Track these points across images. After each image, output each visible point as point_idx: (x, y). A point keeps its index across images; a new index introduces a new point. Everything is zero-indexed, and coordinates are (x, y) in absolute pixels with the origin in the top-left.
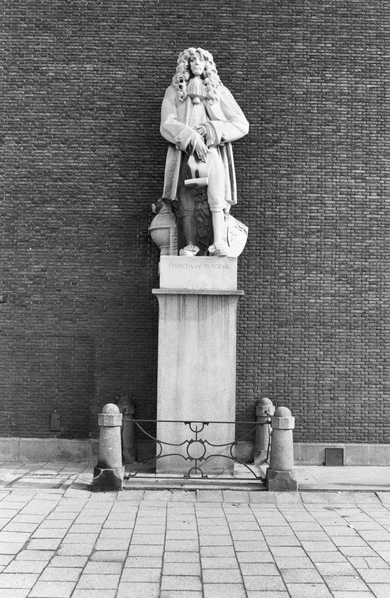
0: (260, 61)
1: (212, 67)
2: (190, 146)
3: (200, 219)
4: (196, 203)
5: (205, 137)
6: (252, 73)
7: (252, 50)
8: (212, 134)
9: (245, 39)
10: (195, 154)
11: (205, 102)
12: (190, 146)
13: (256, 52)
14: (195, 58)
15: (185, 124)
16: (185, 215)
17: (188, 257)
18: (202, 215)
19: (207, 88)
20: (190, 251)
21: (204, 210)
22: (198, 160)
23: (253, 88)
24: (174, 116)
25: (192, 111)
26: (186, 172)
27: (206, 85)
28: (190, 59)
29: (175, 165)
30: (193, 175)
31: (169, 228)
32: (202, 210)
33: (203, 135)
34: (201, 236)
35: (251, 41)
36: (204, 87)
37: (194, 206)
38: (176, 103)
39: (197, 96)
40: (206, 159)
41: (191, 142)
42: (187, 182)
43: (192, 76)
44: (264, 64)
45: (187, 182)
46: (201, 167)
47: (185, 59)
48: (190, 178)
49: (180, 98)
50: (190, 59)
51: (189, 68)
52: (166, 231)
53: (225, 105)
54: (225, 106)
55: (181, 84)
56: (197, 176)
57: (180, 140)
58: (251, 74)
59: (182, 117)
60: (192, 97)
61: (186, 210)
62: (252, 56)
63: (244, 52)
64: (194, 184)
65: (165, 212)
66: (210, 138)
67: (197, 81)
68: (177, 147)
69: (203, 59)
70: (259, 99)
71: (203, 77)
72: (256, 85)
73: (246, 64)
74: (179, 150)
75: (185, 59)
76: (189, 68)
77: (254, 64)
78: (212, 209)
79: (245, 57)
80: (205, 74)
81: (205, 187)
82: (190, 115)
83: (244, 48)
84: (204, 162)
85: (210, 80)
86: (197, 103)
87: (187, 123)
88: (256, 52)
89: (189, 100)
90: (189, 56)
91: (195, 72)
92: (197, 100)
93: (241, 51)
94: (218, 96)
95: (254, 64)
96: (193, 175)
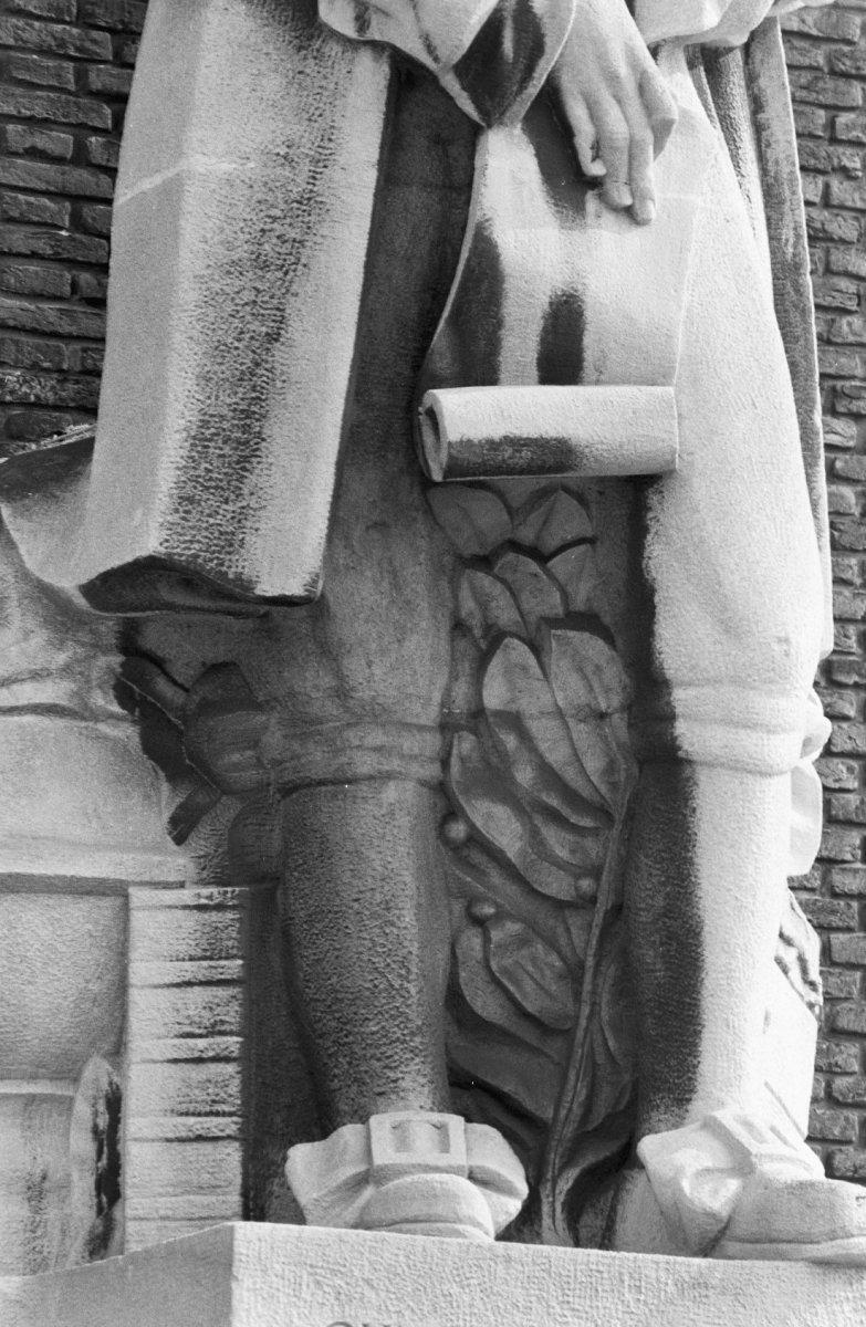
3: (503, 828)
4: (477, 644)
10: (551, 128)
16: (365, 764)
17: (134, 1258)
18: (524, 775)
20: (464, 1171)
21: (545, 732)
22: (571, 179)
26: (435, 305)
29: (307, 205)
30: (521, 338)
31: (116, 891)
32: (515, 721)
34: (486, 1004)
37: (442, 681)
42: (469, 414)
45: (469, 414)
46: (600, 263)
48: (480, 369)
52: (82, 917)
56: (562, 360)
61: (377, 714)
64: (540, 444)
65: (29, 693)
78: (691, 735)
81: (633, 496)
84: (630, 214)
96: (521, 338)
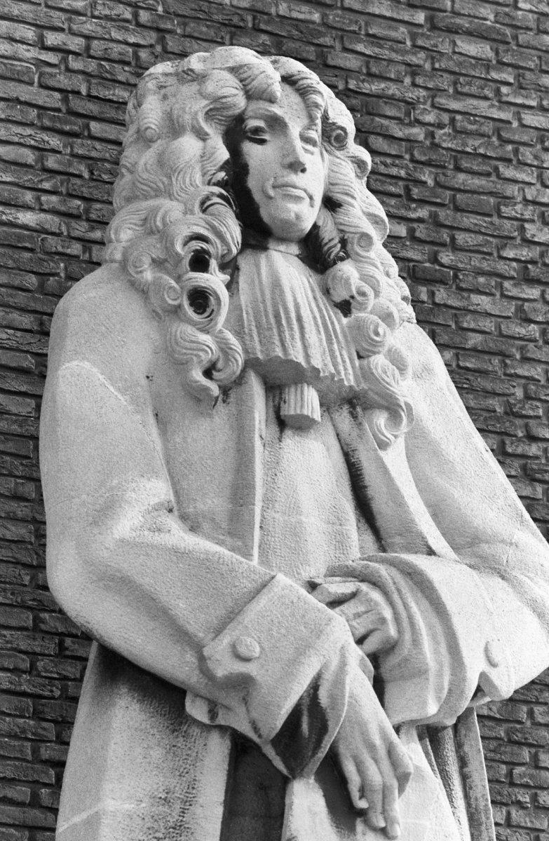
0: (509, 172)
1: (364, 208)
2: (312, 714)
5: (375, 658)
6: (461, 238)
7: (459, 94)
8: (430, 652)
9: (420, 17)
11: (343, 418)
12: (312, 714)
13: (483, 107)
14: (276, 124)
15: (248, 555)
19: (359, 328)
23: (474, 340)
24: (159, 489)
25: (274, 466)
27: (345, 307)
28: (240, 119)
33: (372, 644)
35: (453, 31)
36: (341, 322)
38: (156, 397)
39: (301, 375)
40: (295, 834)
41: (315, 687)
43: (258, 233)
44: (530, 193)
47: (209, 115)
49: (197, 375)
50: (240, 119)
51: (236, 185)
53: (436, 453)
54: (436, 453)
55: (201, 279)
57: (251, 669)
58: (454, 247)
59: (214, 502)
60: (279, 380)
62: (458, 132)
63: (411, 95)
66: (422, 672)
67: (285, 265)
68: (196, 710)
69: (315, 134)
70: (510, 413)
71: (316, 254)
72: (488, 325)
73: (427, 177)
74: (214, 727)
75: (209, 115)
76: (236, 185)
77: (477, 182)
79: (418, 133)
80: (329, 233)
82: (268, 501)
83: (414, 70)
85: (365, 278)
86: (302, 425)
87: (256, 552)
88: (483, 107)
89: (256, 389)
90: (240, 102)
91: (274, 211)
92: (309, 401)
93: (393, 89)
94: (404, 389)
95: (477, 182)
